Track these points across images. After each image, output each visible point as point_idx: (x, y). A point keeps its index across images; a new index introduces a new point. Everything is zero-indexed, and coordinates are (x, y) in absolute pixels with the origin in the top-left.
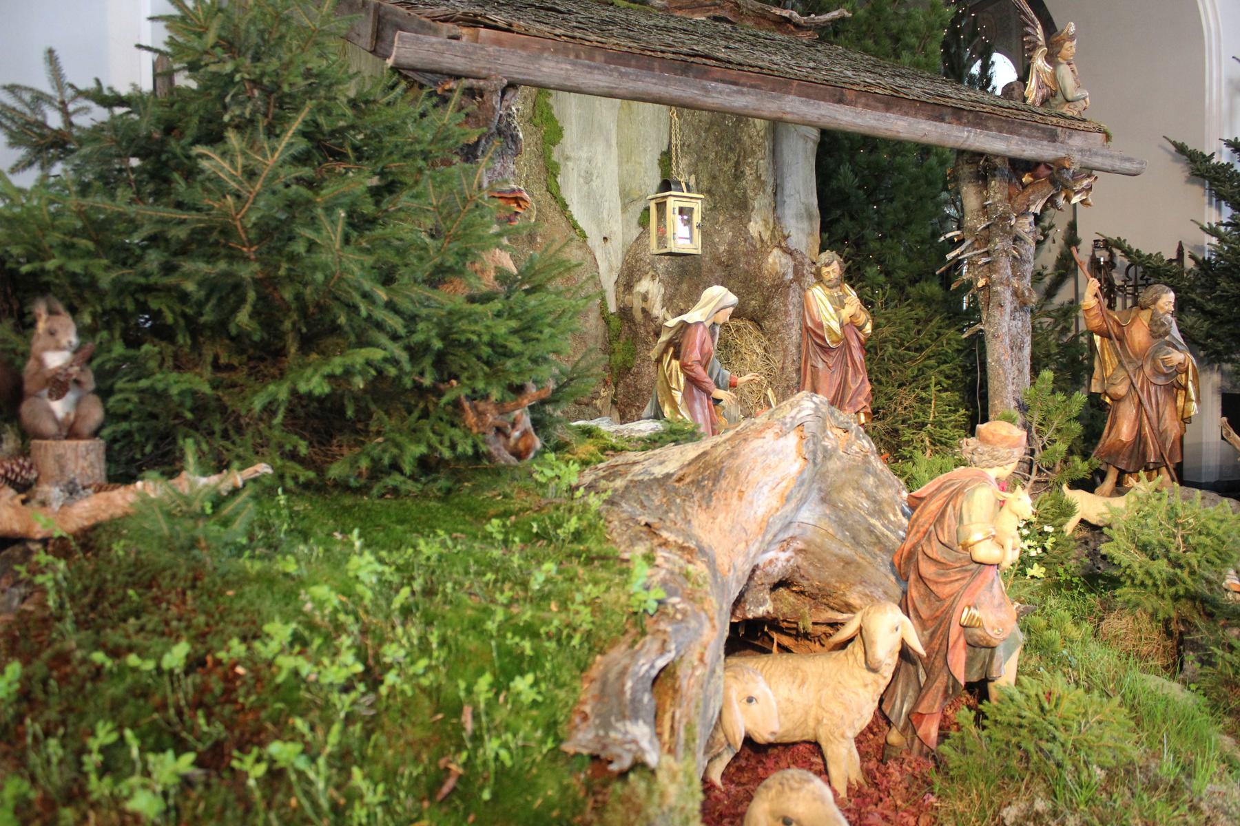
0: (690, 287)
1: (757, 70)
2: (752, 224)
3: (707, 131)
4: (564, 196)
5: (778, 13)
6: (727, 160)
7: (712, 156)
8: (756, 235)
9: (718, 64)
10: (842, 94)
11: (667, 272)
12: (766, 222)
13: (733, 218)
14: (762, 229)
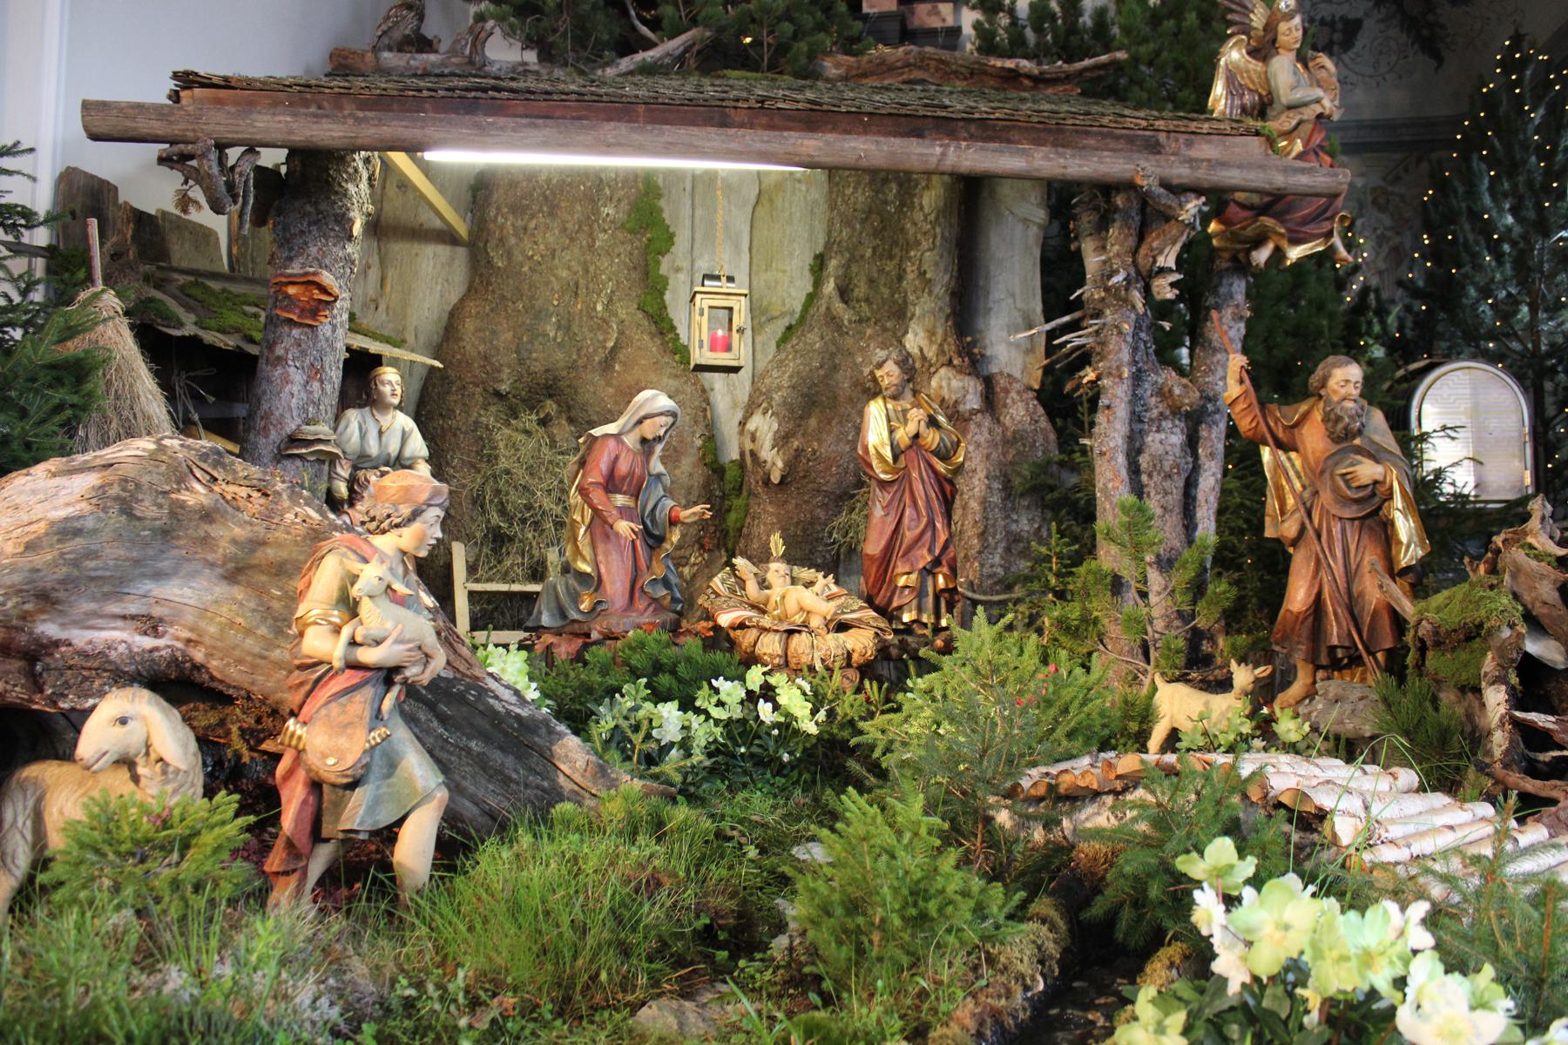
0: (820, 422)
1: (574, 97)
2: (910, 336)
3: (864, 221)
4: (671, 315)
5: (999, 63)
6: (891, 257)
7: (869, 253)
8: (916, 351)
9: (512, 96)
10: (726, 116)
11: (784, 403)
12: (931, 333)
13: (885, 330)
14: (924, 343)
